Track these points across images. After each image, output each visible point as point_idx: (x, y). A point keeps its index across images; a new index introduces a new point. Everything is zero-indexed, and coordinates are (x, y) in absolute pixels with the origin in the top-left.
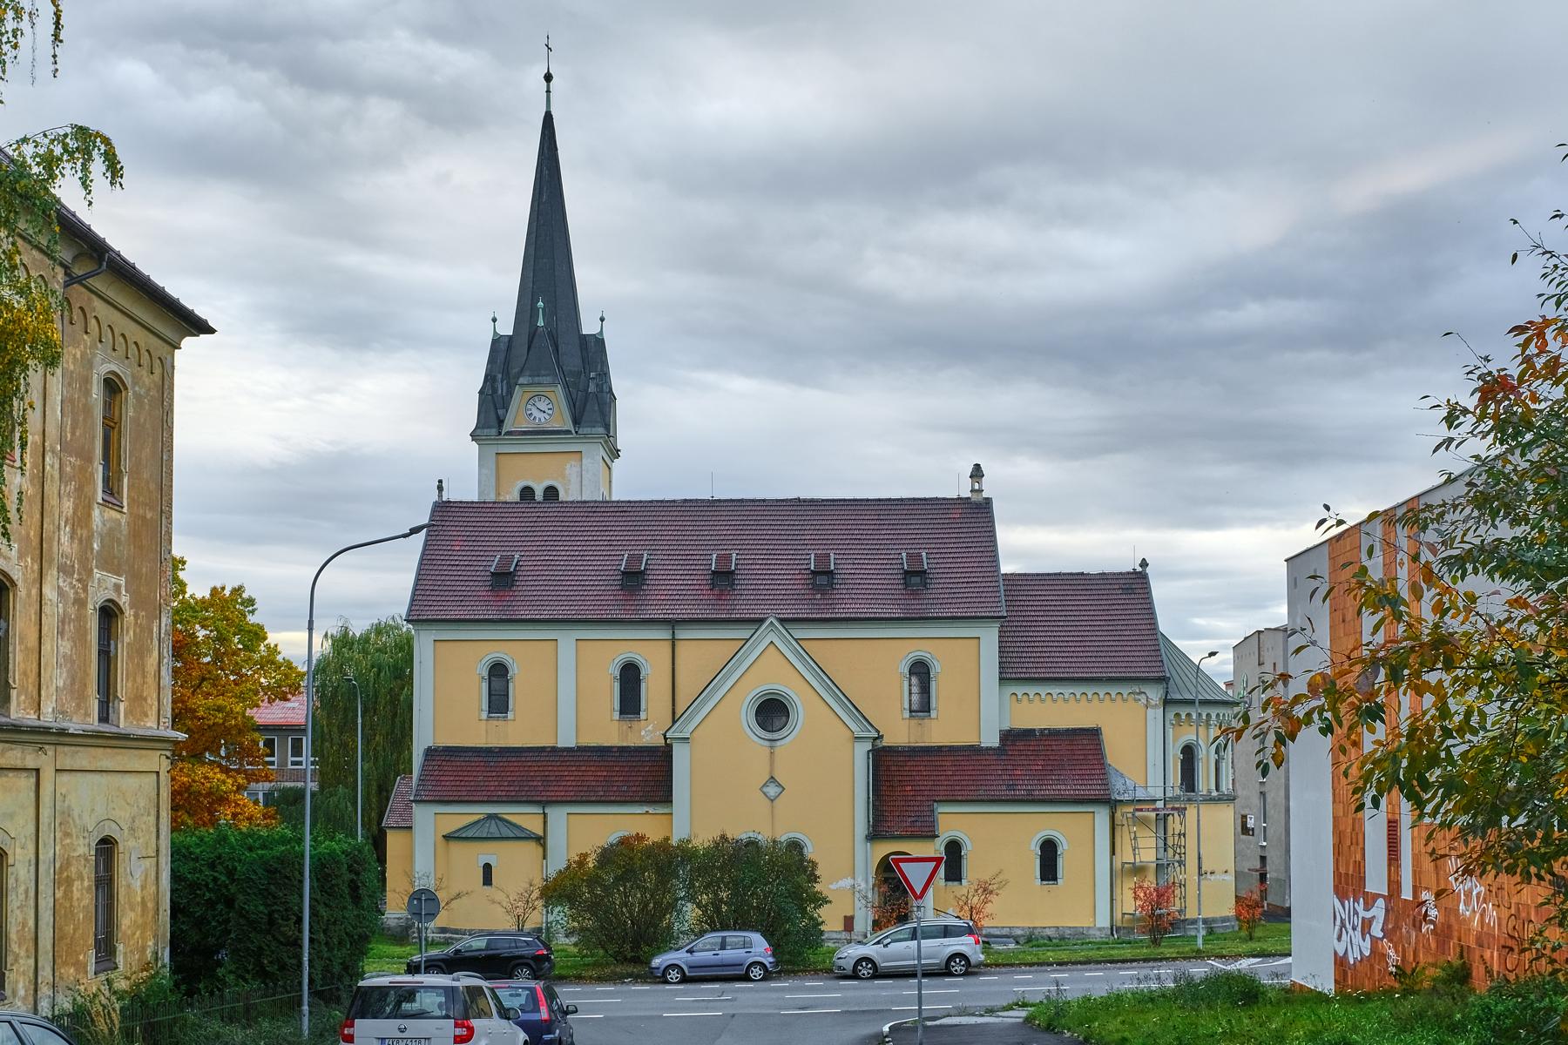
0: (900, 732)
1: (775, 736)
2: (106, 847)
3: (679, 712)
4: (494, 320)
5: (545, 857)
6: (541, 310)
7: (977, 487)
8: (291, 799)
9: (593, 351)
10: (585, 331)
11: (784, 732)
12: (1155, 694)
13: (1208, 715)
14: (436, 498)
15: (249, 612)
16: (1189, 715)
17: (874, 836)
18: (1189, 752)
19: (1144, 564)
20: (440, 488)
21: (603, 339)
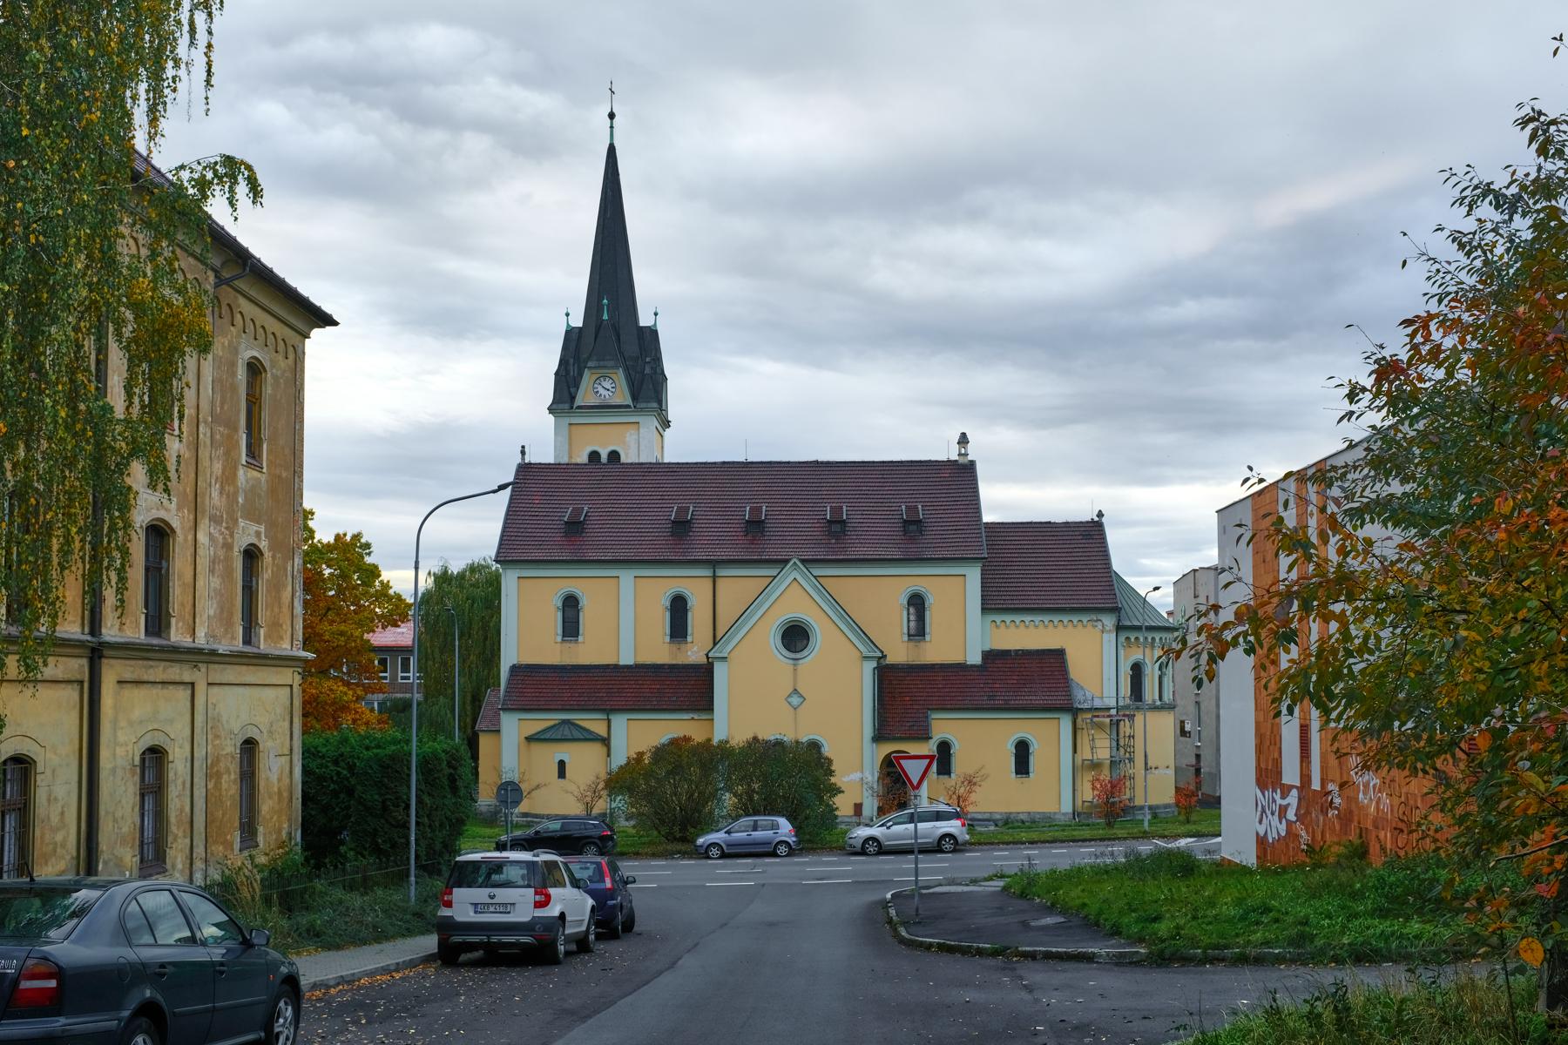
0: (899, 652)
1: (798, 656)
2: (249, 746)
3: (718, 637)
4: (567, 315)
5: (609, 755)
7: (963, 451)
9: (649, 339)
10: (642, 324)
11: (805, 652)
12: (1109, 621)
13: (1153, 639)
16: (1137, 638)
17: (879, 737)
18: (1137, 670)
19: (1100, 514)
20: (523, 453)
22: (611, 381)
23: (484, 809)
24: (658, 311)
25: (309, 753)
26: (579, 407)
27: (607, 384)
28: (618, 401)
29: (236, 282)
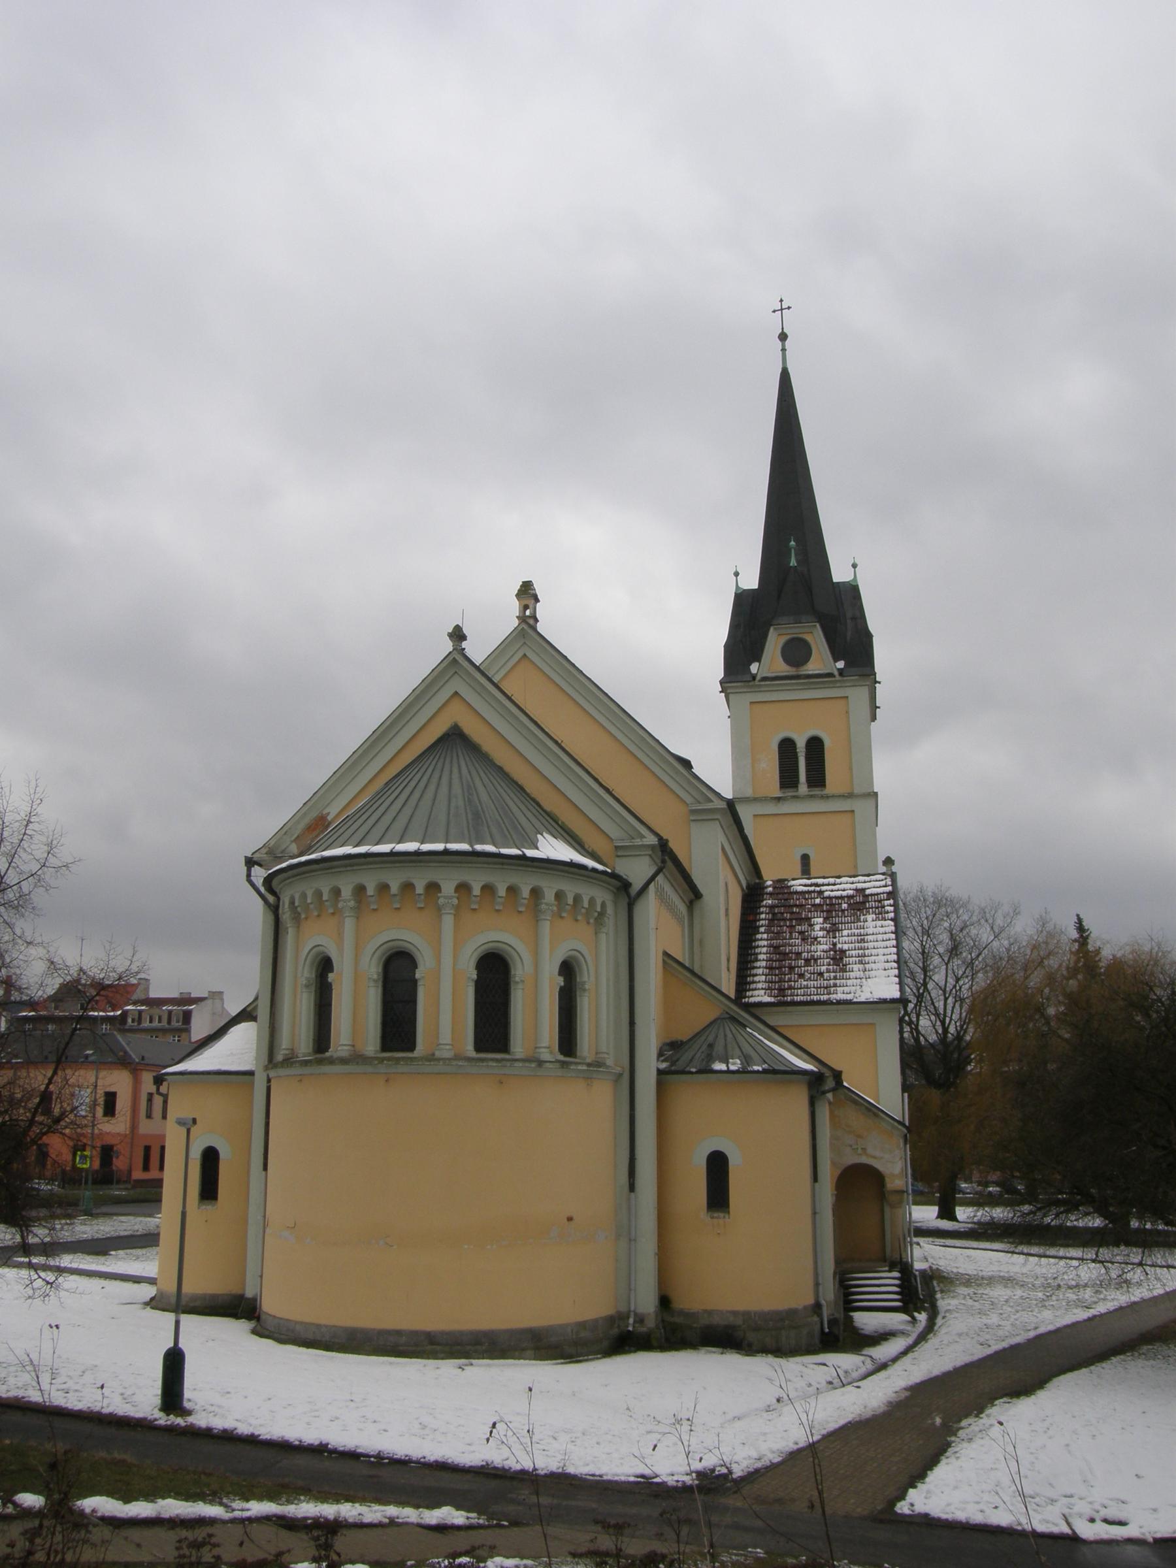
4: (737, 574)
6: (793, 551)
8: (422, 1516)
14: (335, 1548)
21: (858, 585)
23: (1048, 1011)
25: (698, 1313)
29: (687, 965)
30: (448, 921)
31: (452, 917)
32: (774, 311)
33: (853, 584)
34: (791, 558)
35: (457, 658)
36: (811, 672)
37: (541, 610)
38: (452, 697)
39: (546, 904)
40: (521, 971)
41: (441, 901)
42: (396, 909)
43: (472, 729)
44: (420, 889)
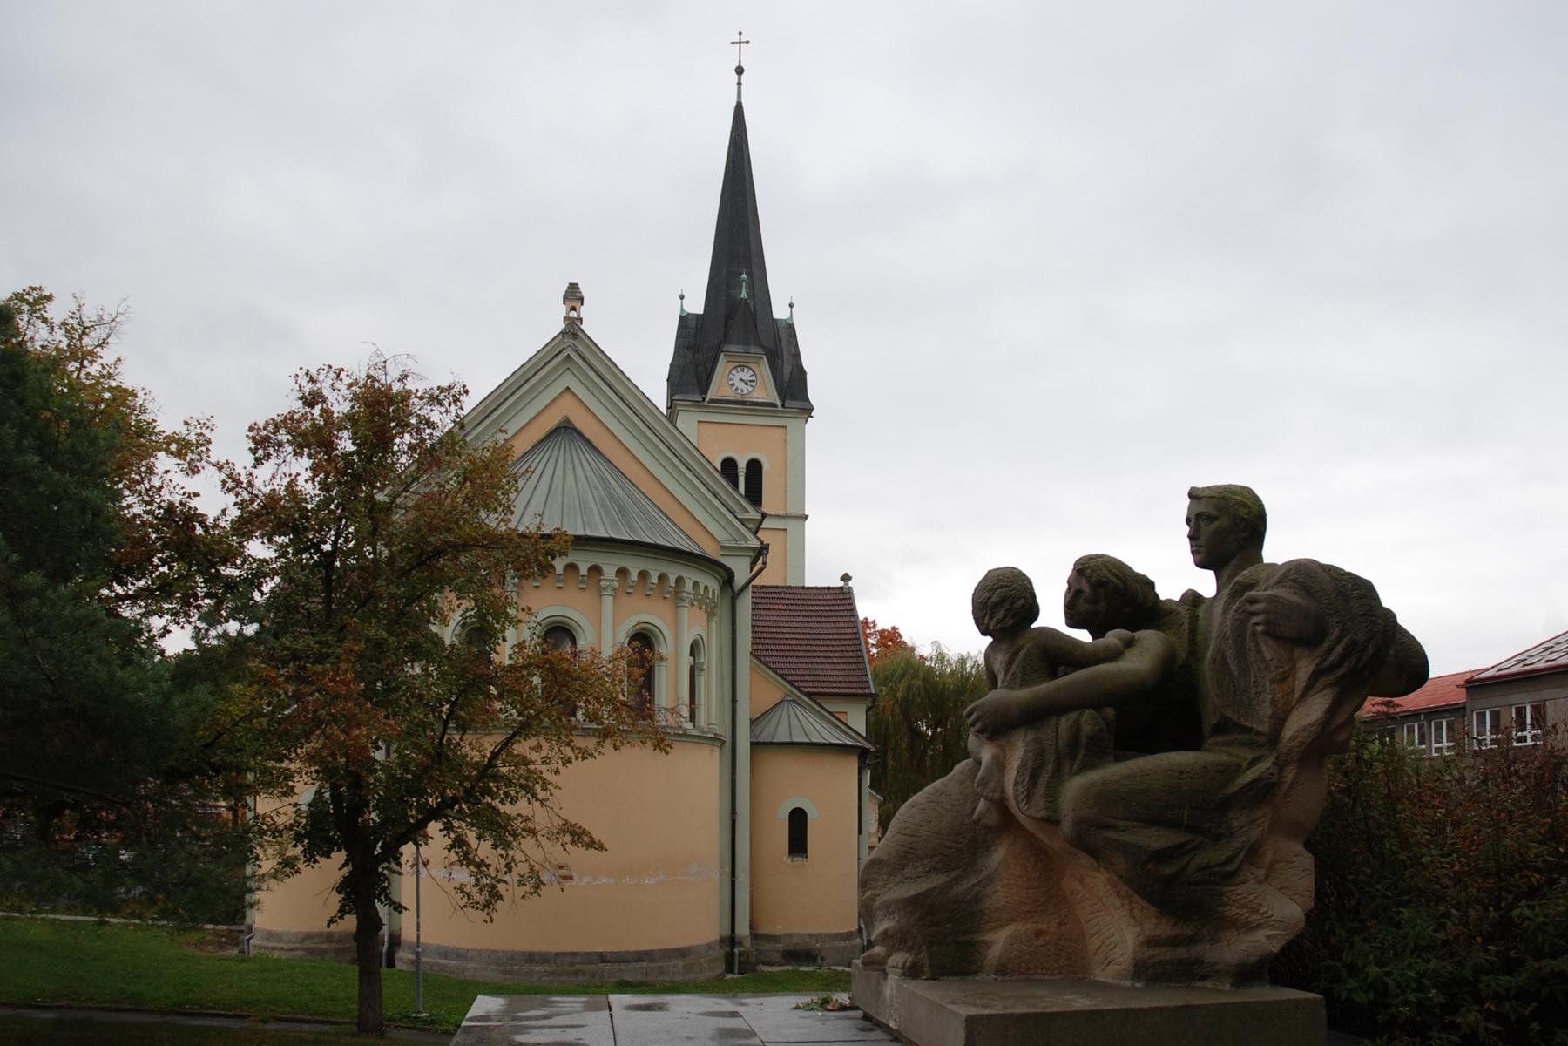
4: (682, 297)
6: (744, 284)
13: (680, 580)
15: (149, 632)
22: (751, 373)
24: (793, 302)
25: (780, 936)
26: (713, 401)
27: (746, 375)
28: (758, 396)
30: (608, 602)
31: (611, 598)
32: (733, 43)
33: (790, 322)
34: (741, 290)
35: (571, 355)
36: (755, 400)
37: (584, 311)
38: (563, 392)
39: (686, 592)
40: (666, 648)
41: (603, 583)
42: (581, 588)
43: (582, 423)
44: (584, 571)
